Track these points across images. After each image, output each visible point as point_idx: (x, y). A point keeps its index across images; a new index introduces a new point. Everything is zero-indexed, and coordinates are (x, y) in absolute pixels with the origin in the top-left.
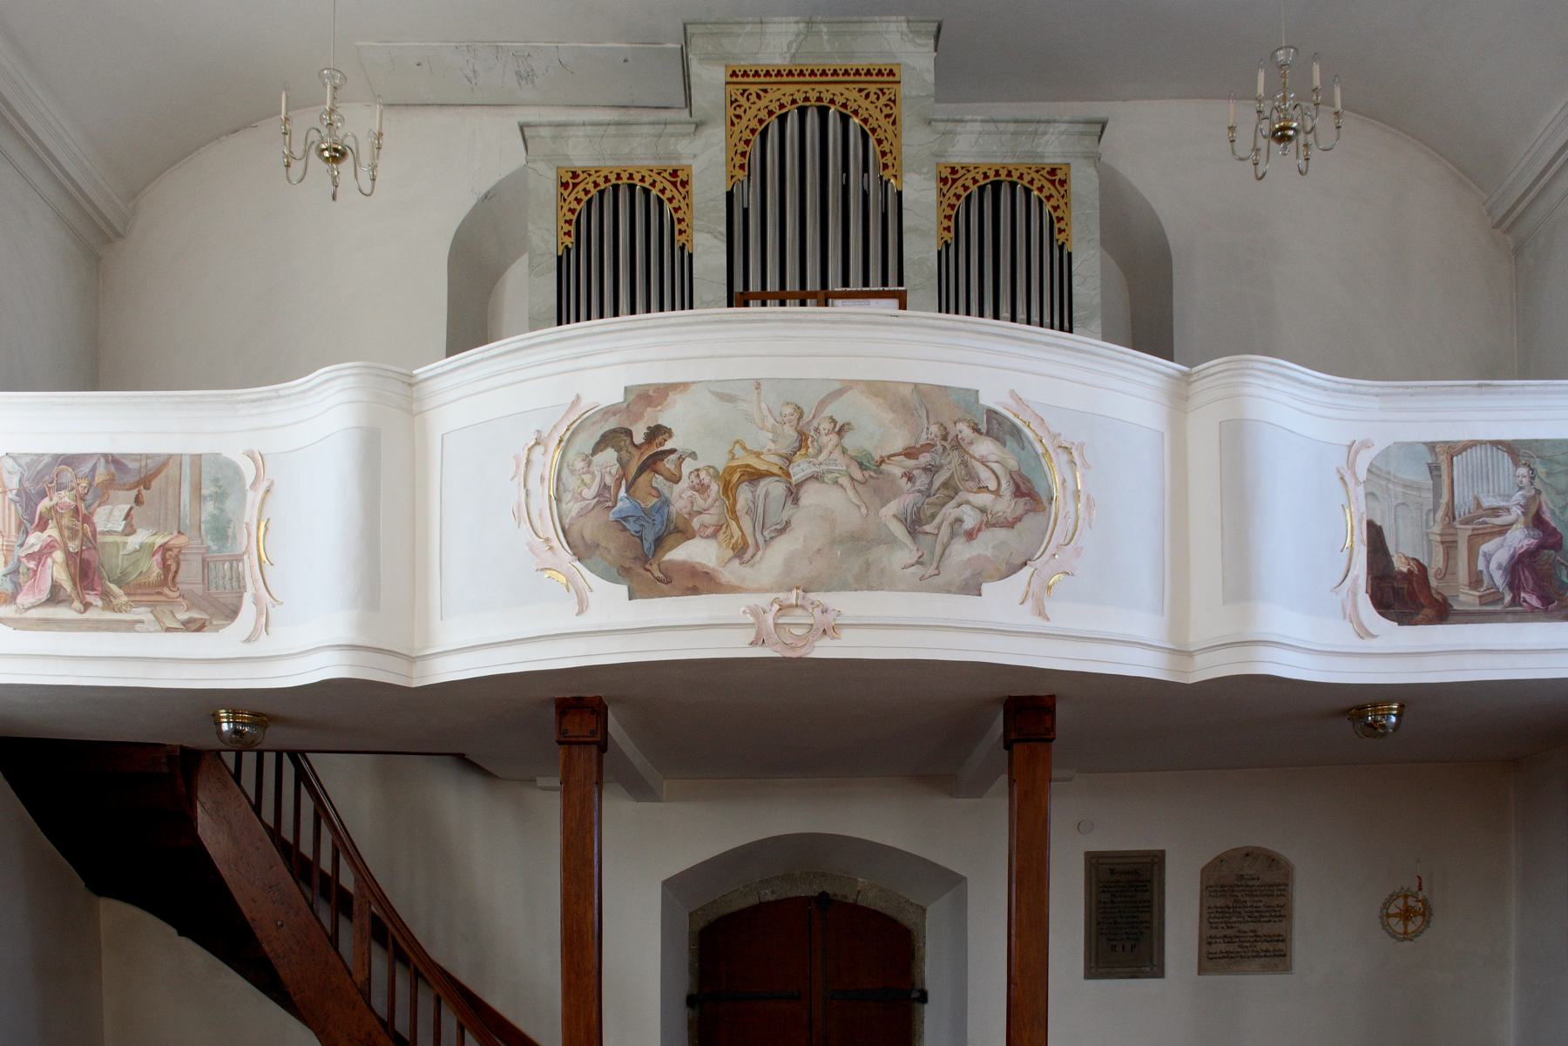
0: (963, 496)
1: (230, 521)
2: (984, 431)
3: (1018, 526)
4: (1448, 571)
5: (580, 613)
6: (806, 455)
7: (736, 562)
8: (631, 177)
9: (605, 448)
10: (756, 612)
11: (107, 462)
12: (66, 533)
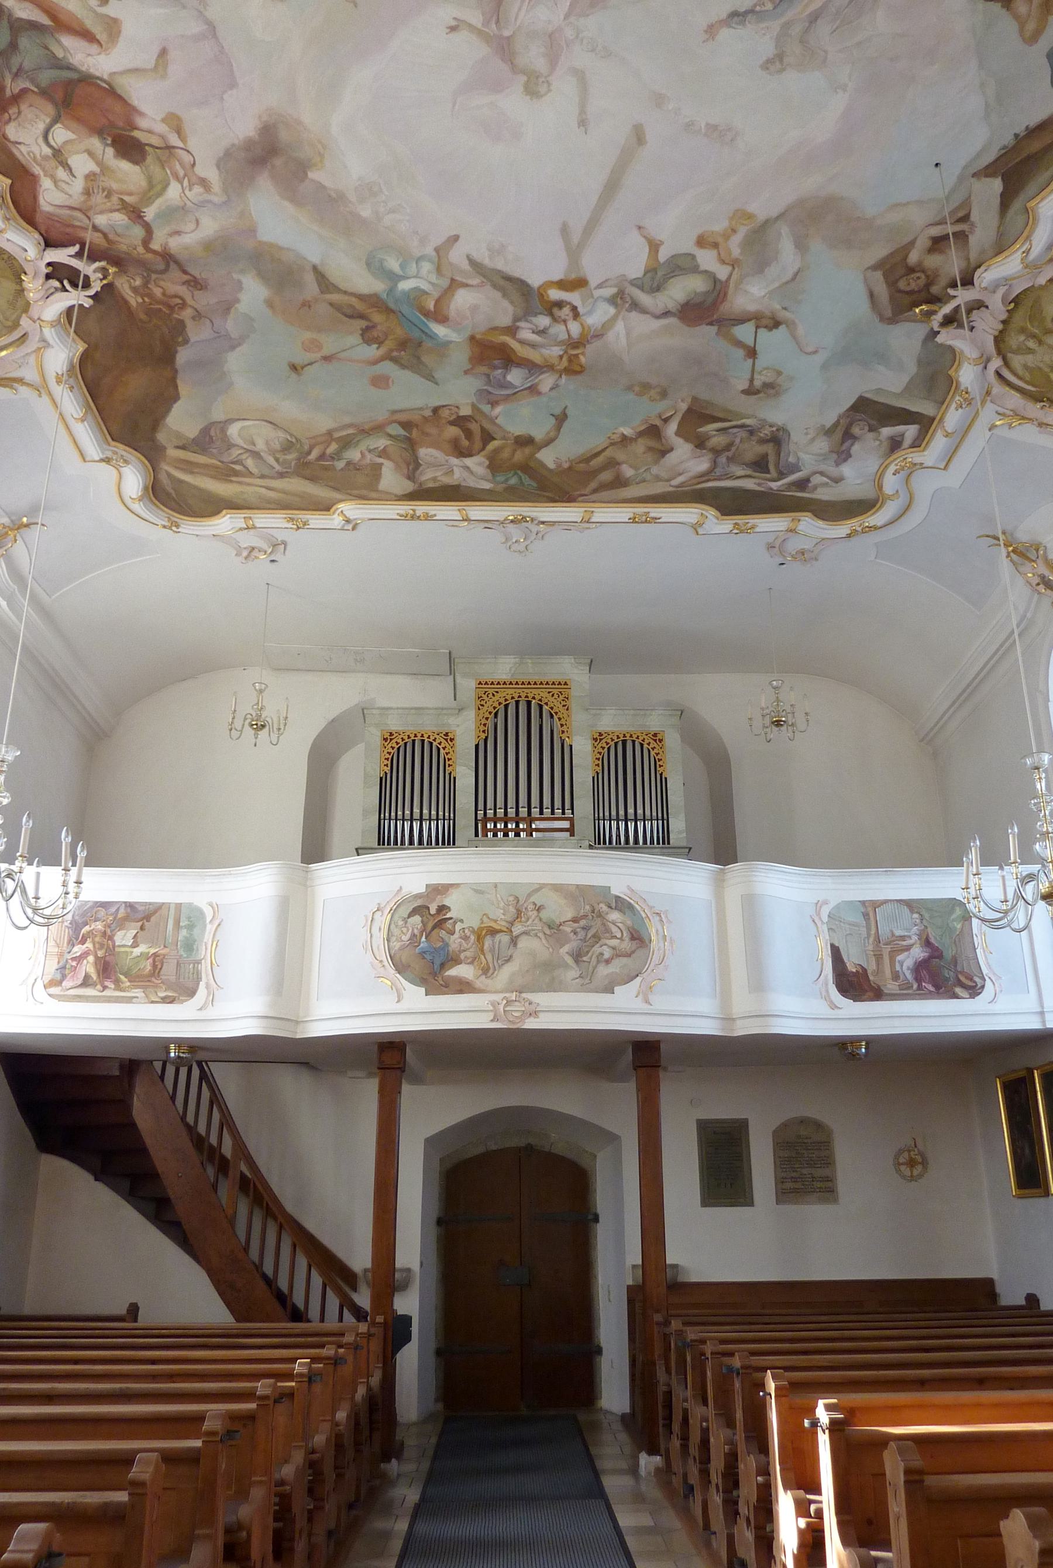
0: (603, 941)
1: (195, 941)
2: (614, 907)
3: (634, 955)
4: (879, 971)
5: (398, 1001)
6: (521, 921)
7: (484, 976)
8: (422, 736)
9: (415, 915)
10: (495, 1004)
11: (126, 906)
12: (97, 946)
